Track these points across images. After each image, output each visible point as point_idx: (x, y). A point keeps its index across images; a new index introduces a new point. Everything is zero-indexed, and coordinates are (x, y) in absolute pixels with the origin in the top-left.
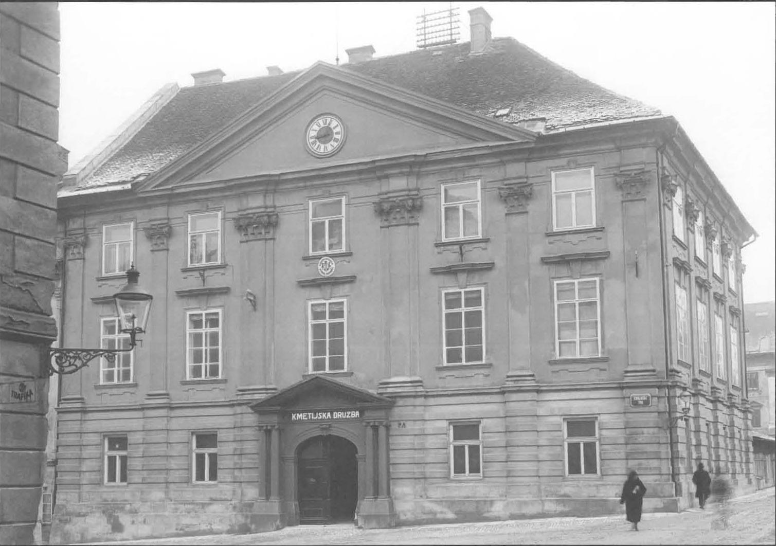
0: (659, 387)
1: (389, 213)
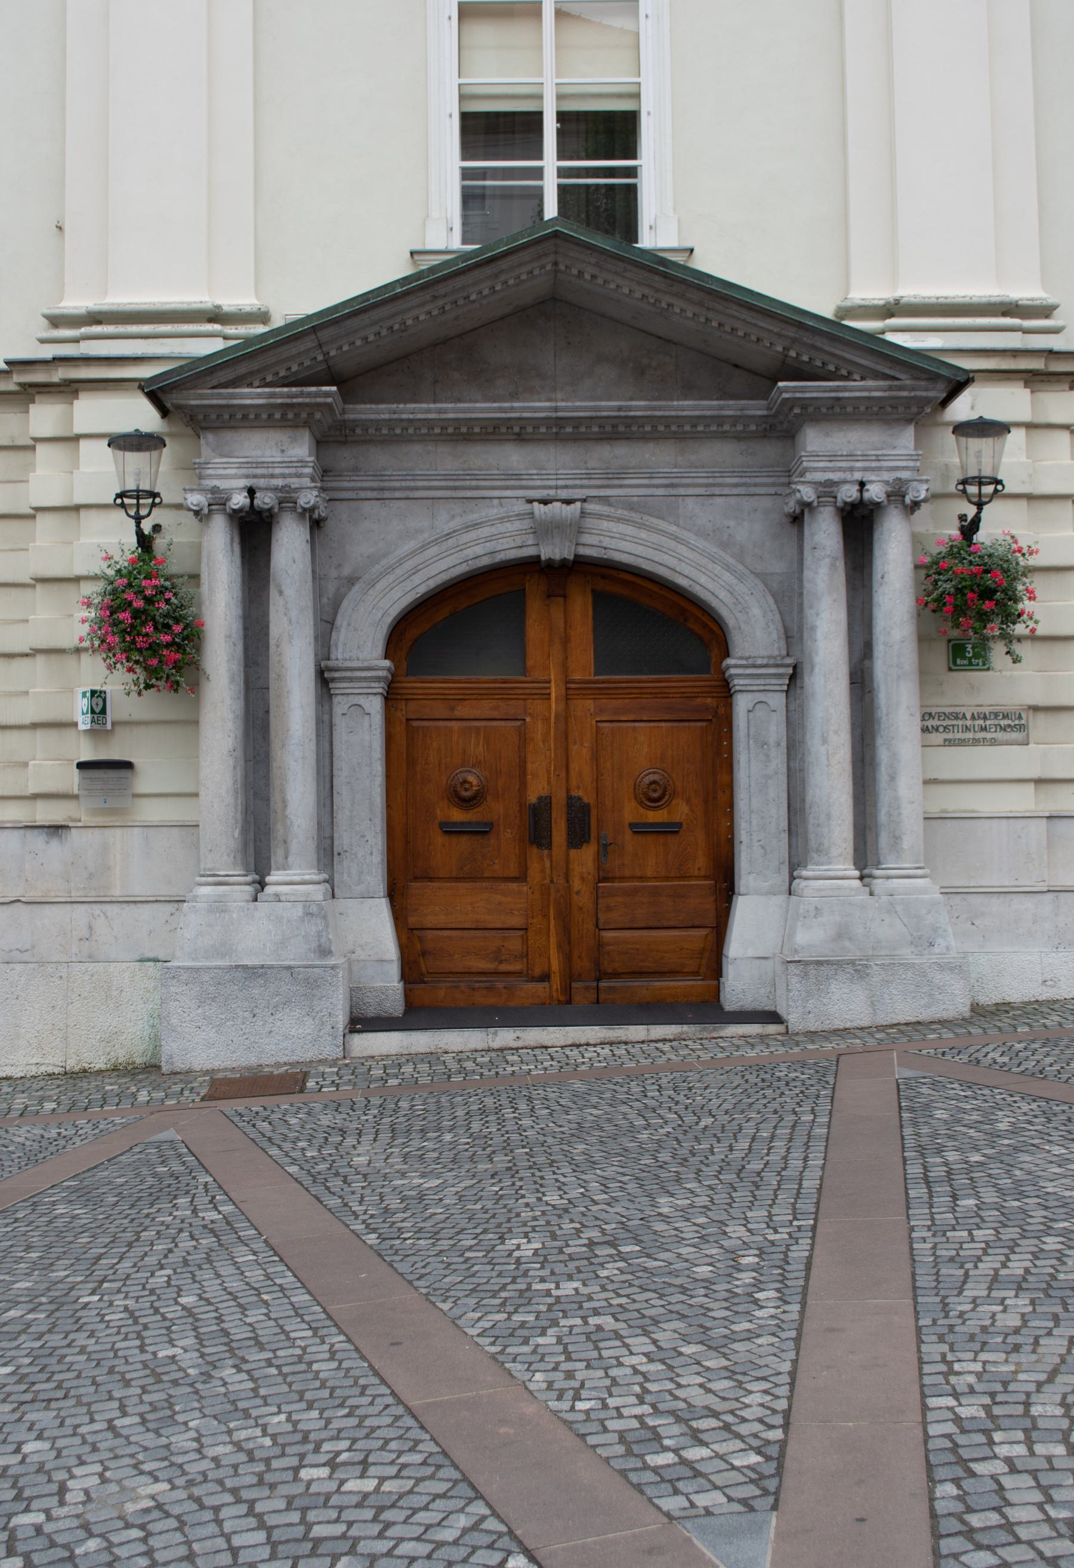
0: (1034, 379)
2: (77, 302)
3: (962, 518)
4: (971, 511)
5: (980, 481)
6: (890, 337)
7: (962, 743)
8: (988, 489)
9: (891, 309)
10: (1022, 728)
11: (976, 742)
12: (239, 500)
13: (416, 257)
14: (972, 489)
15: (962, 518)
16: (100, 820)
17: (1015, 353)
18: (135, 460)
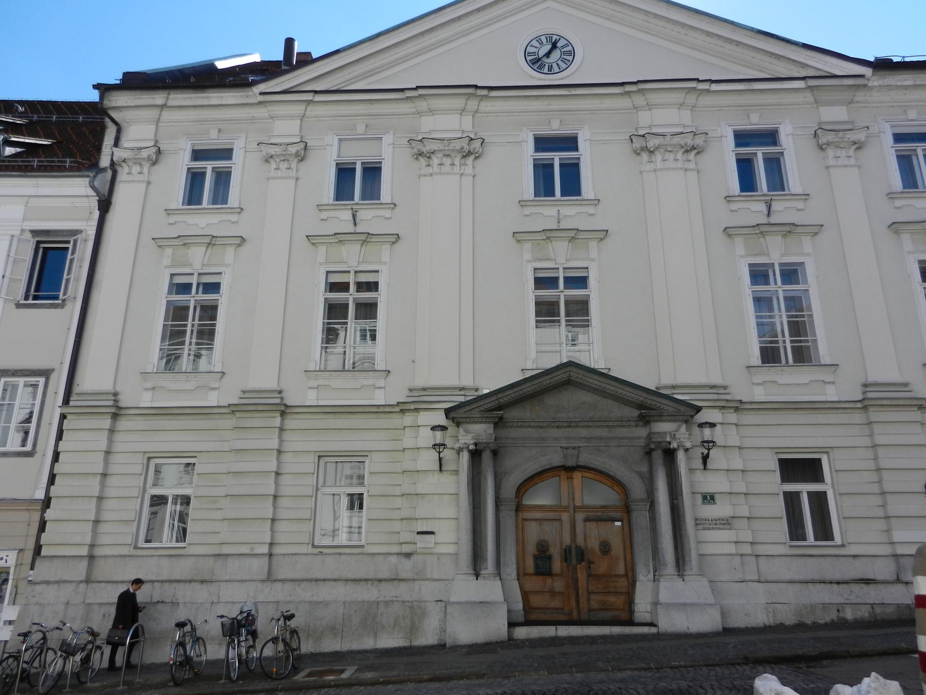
1: (651, 152)
2: (420, 382)
3: (703, 453)
4: (706, 452)
5: (708, 442)
6: (675, 396)
7: (709, 529)
8: (711, 444)
9: (674, 387)
10: (729, 524)
11: (713, 529)
12: (471, 447)
13: (452, 415)
14: (706, 444)
15: (703, 453)
16: (531, 549)
17: (715, 400)
18: (439, 434)
